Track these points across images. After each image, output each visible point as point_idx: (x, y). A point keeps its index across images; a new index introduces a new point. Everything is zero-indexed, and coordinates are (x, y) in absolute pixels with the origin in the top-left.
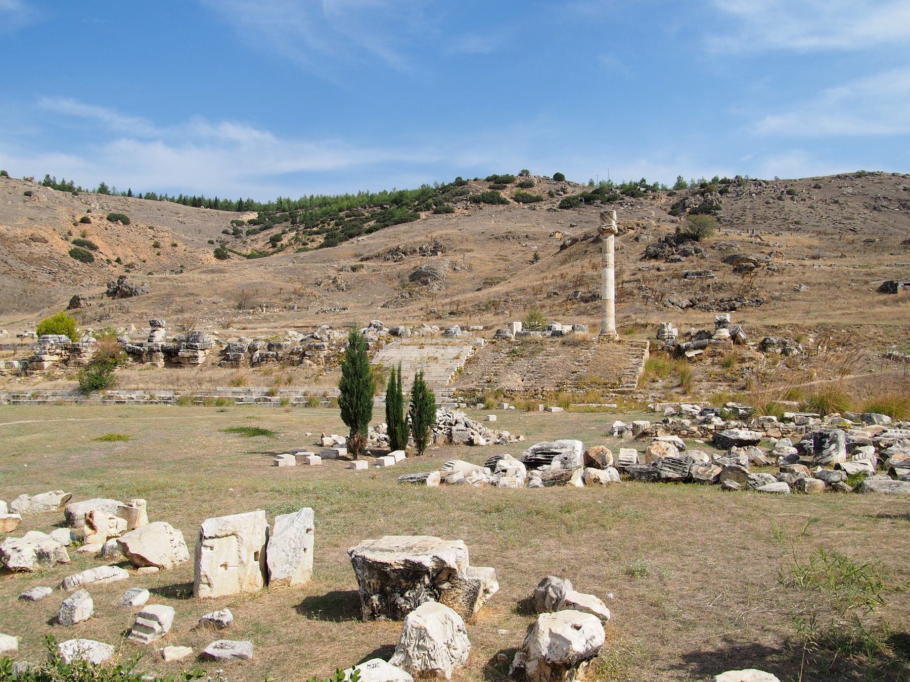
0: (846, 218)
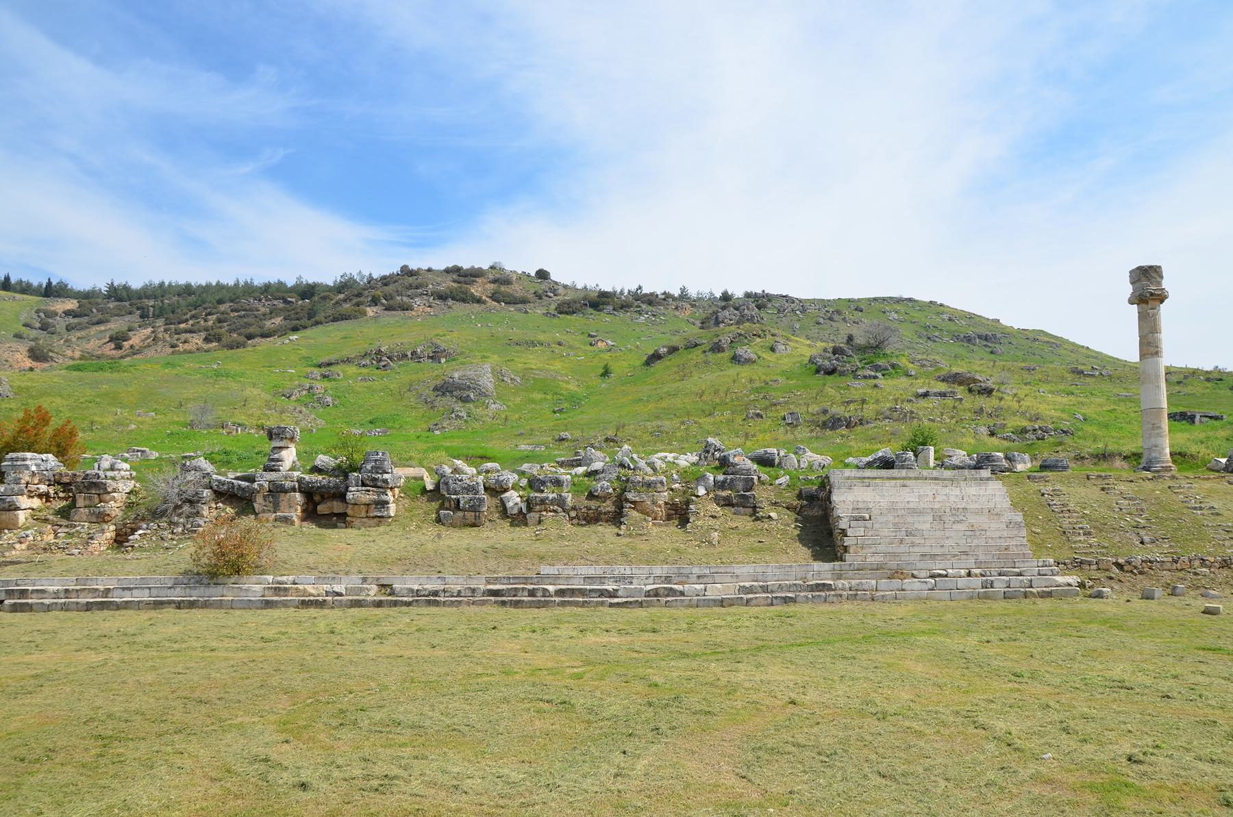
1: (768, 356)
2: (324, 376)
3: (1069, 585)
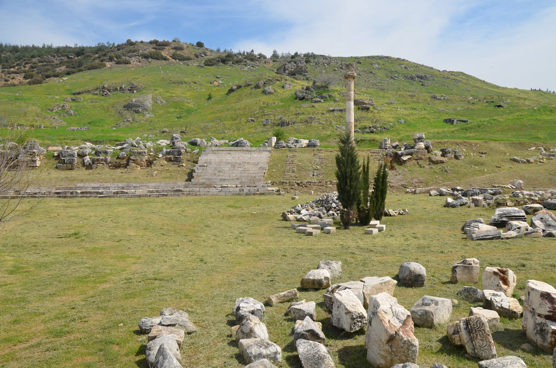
0: (379, 83)
1: (280, 91)
2: (73, 100)
3: (273, 190)
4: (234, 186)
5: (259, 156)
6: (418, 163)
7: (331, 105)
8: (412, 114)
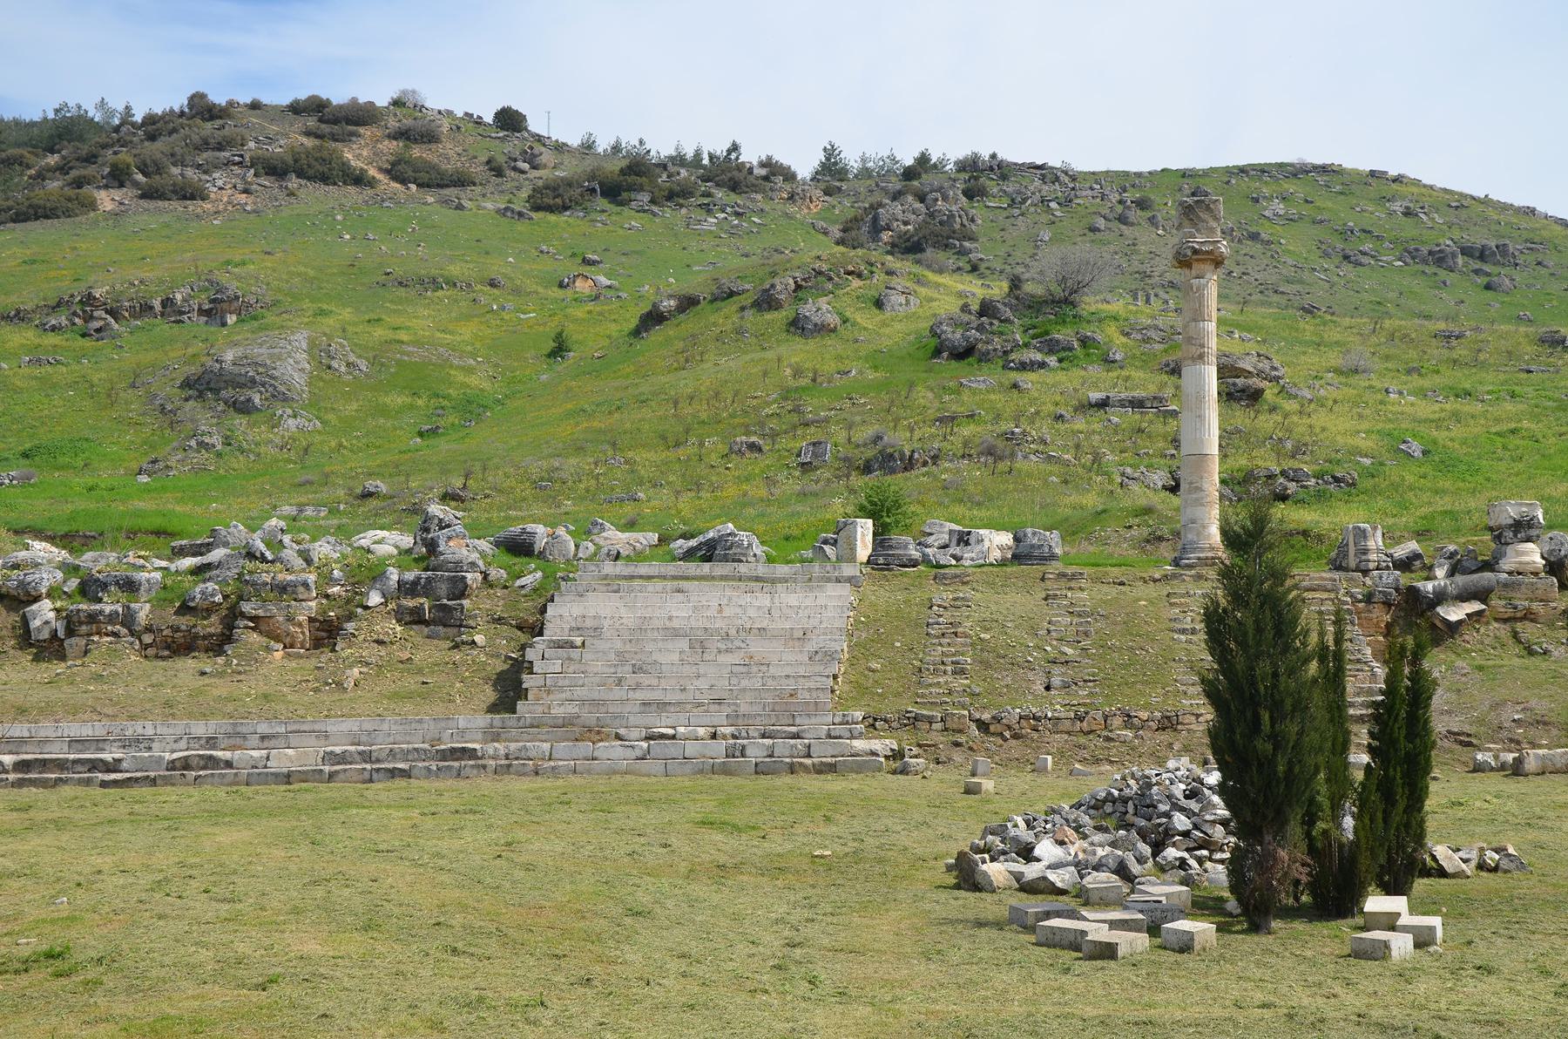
1: (866, 319)
3: (873, 753)
4: (701, 731)
5: (808, 602)
6: (1515, 635)
7: (1094, 382)
8: (1457, 416)
